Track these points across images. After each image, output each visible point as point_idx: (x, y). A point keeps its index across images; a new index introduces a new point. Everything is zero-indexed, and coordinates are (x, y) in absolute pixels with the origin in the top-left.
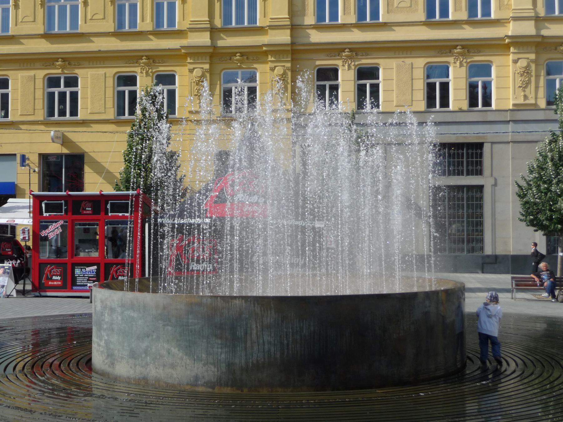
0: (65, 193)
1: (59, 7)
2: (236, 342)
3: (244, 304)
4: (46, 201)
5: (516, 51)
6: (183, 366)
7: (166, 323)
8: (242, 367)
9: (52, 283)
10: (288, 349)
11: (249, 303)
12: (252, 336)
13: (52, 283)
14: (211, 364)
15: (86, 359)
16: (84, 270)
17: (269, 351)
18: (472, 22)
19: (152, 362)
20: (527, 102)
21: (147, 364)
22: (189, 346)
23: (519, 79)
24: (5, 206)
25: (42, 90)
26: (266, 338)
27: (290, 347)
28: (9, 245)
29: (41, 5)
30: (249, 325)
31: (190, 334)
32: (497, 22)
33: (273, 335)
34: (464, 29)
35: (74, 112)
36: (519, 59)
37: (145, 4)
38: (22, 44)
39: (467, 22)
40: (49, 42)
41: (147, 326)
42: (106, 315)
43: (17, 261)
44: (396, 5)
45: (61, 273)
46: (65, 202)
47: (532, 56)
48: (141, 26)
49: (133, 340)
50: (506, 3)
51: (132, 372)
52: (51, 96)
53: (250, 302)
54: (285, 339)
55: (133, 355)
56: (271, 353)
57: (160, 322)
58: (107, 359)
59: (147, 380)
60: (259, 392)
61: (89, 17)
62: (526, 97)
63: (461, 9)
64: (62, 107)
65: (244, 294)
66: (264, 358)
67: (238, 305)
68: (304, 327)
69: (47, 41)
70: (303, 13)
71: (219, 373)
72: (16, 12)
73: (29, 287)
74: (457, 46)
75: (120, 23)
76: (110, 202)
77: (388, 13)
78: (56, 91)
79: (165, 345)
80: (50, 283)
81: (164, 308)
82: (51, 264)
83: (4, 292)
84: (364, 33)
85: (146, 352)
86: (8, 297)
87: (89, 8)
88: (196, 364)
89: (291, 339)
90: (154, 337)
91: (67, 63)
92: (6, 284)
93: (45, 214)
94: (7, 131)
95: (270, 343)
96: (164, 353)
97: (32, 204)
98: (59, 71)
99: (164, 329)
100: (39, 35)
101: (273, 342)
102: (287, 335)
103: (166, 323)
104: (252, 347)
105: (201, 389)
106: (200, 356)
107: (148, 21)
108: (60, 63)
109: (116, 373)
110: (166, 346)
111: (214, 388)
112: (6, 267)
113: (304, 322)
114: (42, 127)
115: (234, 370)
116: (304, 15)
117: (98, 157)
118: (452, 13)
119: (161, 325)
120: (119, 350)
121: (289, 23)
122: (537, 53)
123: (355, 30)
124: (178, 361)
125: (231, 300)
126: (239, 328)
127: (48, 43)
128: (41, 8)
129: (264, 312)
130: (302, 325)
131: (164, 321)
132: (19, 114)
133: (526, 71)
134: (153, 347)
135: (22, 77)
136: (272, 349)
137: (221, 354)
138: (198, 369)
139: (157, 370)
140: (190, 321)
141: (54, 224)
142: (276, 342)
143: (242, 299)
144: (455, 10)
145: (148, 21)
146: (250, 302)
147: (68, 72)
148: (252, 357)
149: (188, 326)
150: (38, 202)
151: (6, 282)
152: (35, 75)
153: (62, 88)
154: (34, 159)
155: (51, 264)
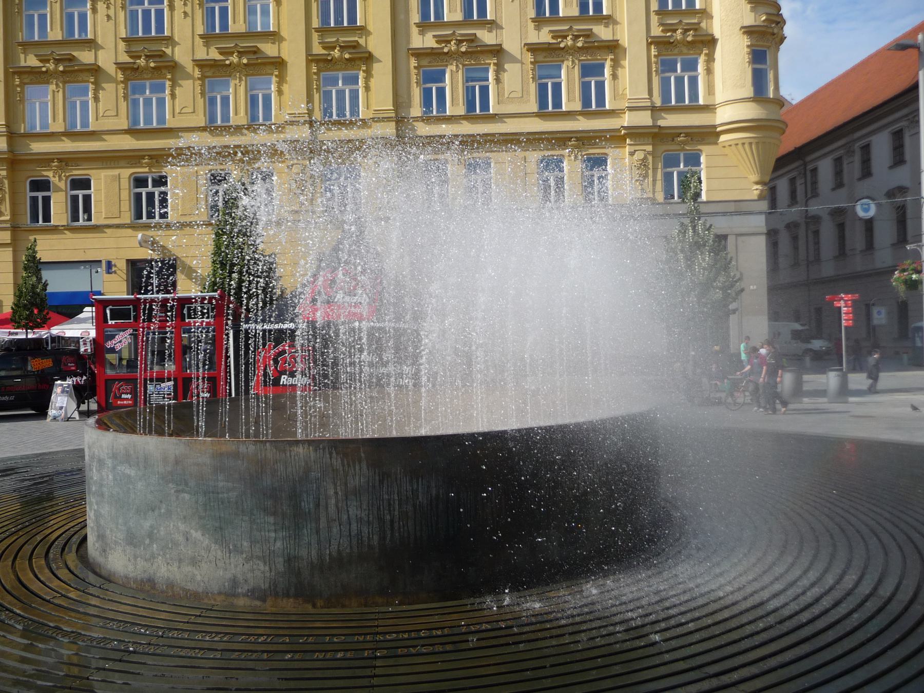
0: (133, 297)
1: (144, 99)
3: (312, 455)
4: (111, 307)
5: (632, 143)
6: (210, 562)
7: (180, 488)
8: (312, 563)
9: (122, 402)
11: (321, 451)
13: (122, 402)
14: (258, 558)
15: (76, 539)
17: (360, 533)
18: (586, 113)
19: (161, 553)
21: (153, 557)
22: (221, 528)
24: (81, 316)
25: (128, 191)
26: (353, 511)
27: (396, 525)
28: (72, 359)
29: (124, 97)
30: (322, 490)
32: (613, 113)
33: (364, 507)
35: (47, 218)
36: (635, 151)
37: (238, 96)
38: (104, 140)
39: (581, 113)
40: (135, 138)
42: (94, 470)
43: (82, 377)
44: (506, 96)
45: (131, 391)
46: (133, 307)
47: (649, 148)
48: (234, 120)
50: (621, 93)
51: (131, 568)
52: (138, 197)
53: (324, 449)
57: (170, 485)
58: (97, 541)
59: (155, 584)
61: (177, 110)
64: (150, 208)
65: (311, 437)
66: (351, 547)
67: (302, 456)
68: (420, 490)
69: (132, 137)
70: (409, 105)
71: (273, 574)
72: (96, 105)
74: (572, 138)
75: (212, 118)
76: (186, 306)
77: (498, 104)
78: (144, 191)
79: (180, 524)
80: (119, 402)
82: (120, 380)
83: (63, 415)
84: (474, 125)
85: (151, 535)
86: (68, 421)
87: (177, 101)
88: (232, 560)
89: (396, 513)
90: (163, 511)
92: (65, 405)
93: (110, 322)
95: (360, 520)
96: (181, 539)
98: (147, 170)
99: (177, 497)
100: (122, 130)
101: (366, 519)
102: (390, 505)
103: (180, 488)
104: (329, 528)
105: (241, 602)
106: (239, 545)
107: (242, 115)
108: (146, 161)
110: (182, 527)
111: (264, 601)
112: (64, 385)
114: (129, 231)
115: (299, 569)
116: (410, 106)
118: (565, 103)
119: (173, 491)
120: (111, 531)
121: (393, 115)
123: (464, 122)
124: (203, 553)
127: (133, 139)
128: (124, 101)
129: (349, 465)
130: (415, 487)
131: (177, 484)
132: (104, 217)
133: (644, 163)
134: (162, 528)
135: (105, 176)
136: (365, 530)
138: (236, 566)
139: (170, 567)
140: (221, 484)
144: (453, 104)
145: (242, 115)
147: (155, 172)
148: (330, 546)
149: (218, 493)
151: (65, 402)
152: (119, 174)
153: (150, 188)
154: (122, 265)
155: (120, 380)
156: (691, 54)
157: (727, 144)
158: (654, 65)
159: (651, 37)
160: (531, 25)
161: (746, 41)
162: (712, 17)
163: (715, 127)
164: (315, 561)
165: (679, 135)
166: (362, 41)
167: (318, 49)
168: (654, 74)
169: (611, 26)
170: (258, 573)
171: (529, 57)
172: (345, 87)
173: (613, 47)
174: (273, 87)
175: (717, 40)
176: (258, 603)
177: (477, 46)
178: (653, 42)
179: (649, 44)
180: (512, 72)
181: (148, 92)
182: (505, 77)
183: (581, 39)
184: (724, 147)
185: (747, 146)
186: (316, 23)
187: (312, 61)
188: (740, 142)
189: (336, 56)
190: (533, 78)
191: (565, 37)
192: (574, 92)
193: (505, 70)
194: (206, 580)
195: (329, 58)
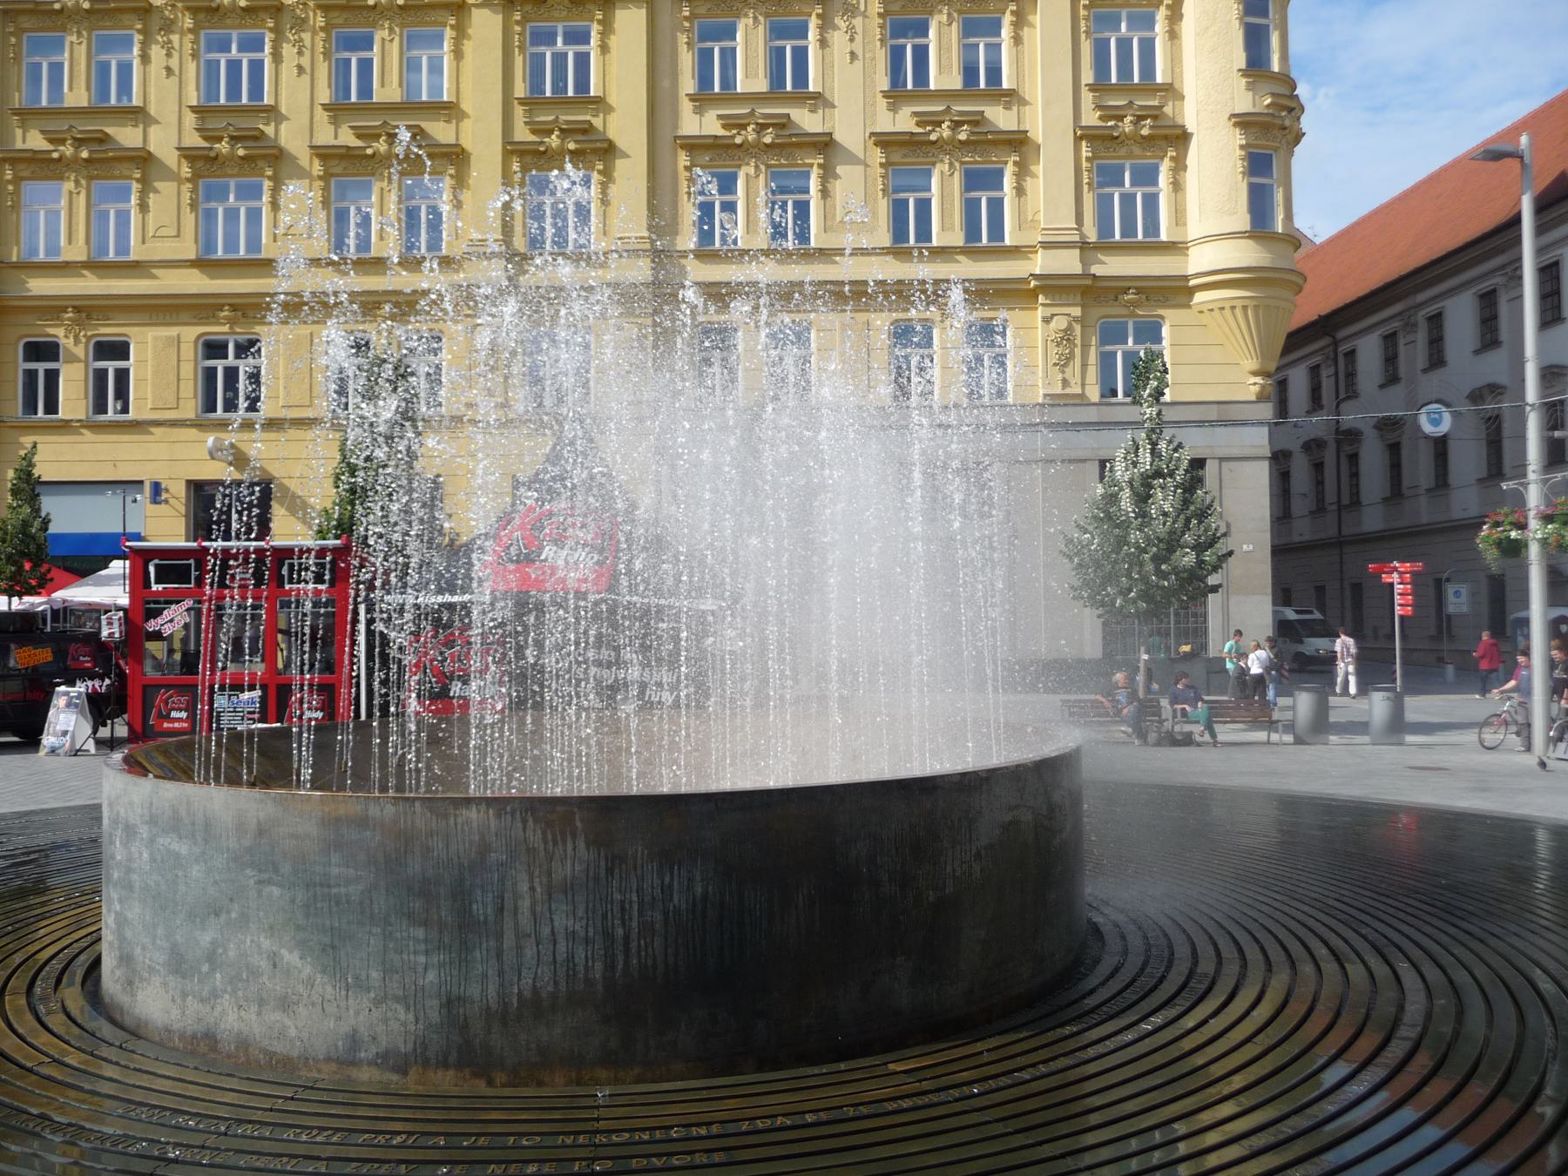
2: (470, 936)
3: (493, 823)
4: (156, 561)
6: (313, 1004)
7: (265, 876)
8: (488, 1008)
10: (627, 950)
11: (509, 817)
12: (520, 916)
14: (397, 999)
16: (234, 699)
17: (571, 958)
19: (229, 989)
20: (1068, 391)
21: (215, 995)
22: (333, 947)
23: (1053, 350)
24: (103, 573)
26: (561, 921)
27: (634, 945)
29: (191, 205)
31: (335, 909)
32: (1016, 252)
33: (581, 912)
34: (958, 262)
36: (1053, 315)
38: (154, 277)
39: (964, 251)
41: (215, 882)
42: (118, 843)
49: (178, 922)
50: (1030, 218)
51: (175, 1013)
52: (210, 374)
53: (513, 813)
54: (617, 922)
55: (179, 965)
56: (575, 965)
57: (249, 872)
58: (118, 967)
60: (540, 1084)
62: (1065, 382)
63: (952, 228)
66: (556, 983)
67: (475, 825)
73: (122, 731)
78: (220, 365)
79: (262, 939)
80: (166, 725)
81: (261, 832)
83: (67, 745)
85: (211, 957)
88: (351, 1001)
89: (635, 924)
90: (233, 915)
91: (240, 313)
92: (71, 729)
93: (155, 587)
94: (126, 438)
96: (264, 964)
97: (127, 571)
98: (226, 328)
99: (260, 893)
101: (582, 934)
102: (623, 910)
103: (265, 876)
104: (519, 948)
105: (365, 1076)
106: (363, 977)
109: (137, 1011)
110: (266, 943)
111: (403, 1070)
113: (676, 872)
117: (293, 485)
119: (252, 881)
120: (144, 948)
122: (1083, 306)
124: (301, 988)
125: (456, 809)
126: (479, 893)
129: (555, 843)
130: (667, 880)
131: (260, 871)
133: (1066, 337)
135: (155, 339)
136: (580, 954)
137: (426, 969)
138: (357, 1013)
140: (335, 871)
141: (173, 606)
142: (591, 934)
143: (488, 808)
146: (513, 813)
147: (242, 333)
148: (519, 980)
149: (329, 886)
150: (140, 562)
151: (73, 723)
154: (178, 490)
155: (168, 686)
156: (1150, 157)
157: (1205, 308)
158: (1085, 174)
159: (1082, 128)
160: (882, 103)
161: (1238, 138)
162: (1182, 98)
163: (1186, 278)
164: (494, 1007)
165: (1126, 290)
166: (597, 122)
167: (522, 134)
168: (1086, 188)
169: (1015, 108)
170: (395, 1026)
171: (878, 156)
172: (1134, 189)
173: (1018, 142)
174: (134, 199)
175: (1191, 135)
176: (395, 1077)
177: (790, 136)
178: (1085, 135)
179: (1078, 140)
180: (849, 180)
181: (232, 198)
182: (838, 187)
183: (965, 127)
184: (1201, 312)
185: (1238, 312)
186: (1088, 76)
187: (1081, 138)
188: (1239, 303)
189: (554, 145)
190: (883, 190)
191: (939, 124)
192: (952, 216)
193: (836, 177)
194: (305, 1035)
195: (542, 149)
